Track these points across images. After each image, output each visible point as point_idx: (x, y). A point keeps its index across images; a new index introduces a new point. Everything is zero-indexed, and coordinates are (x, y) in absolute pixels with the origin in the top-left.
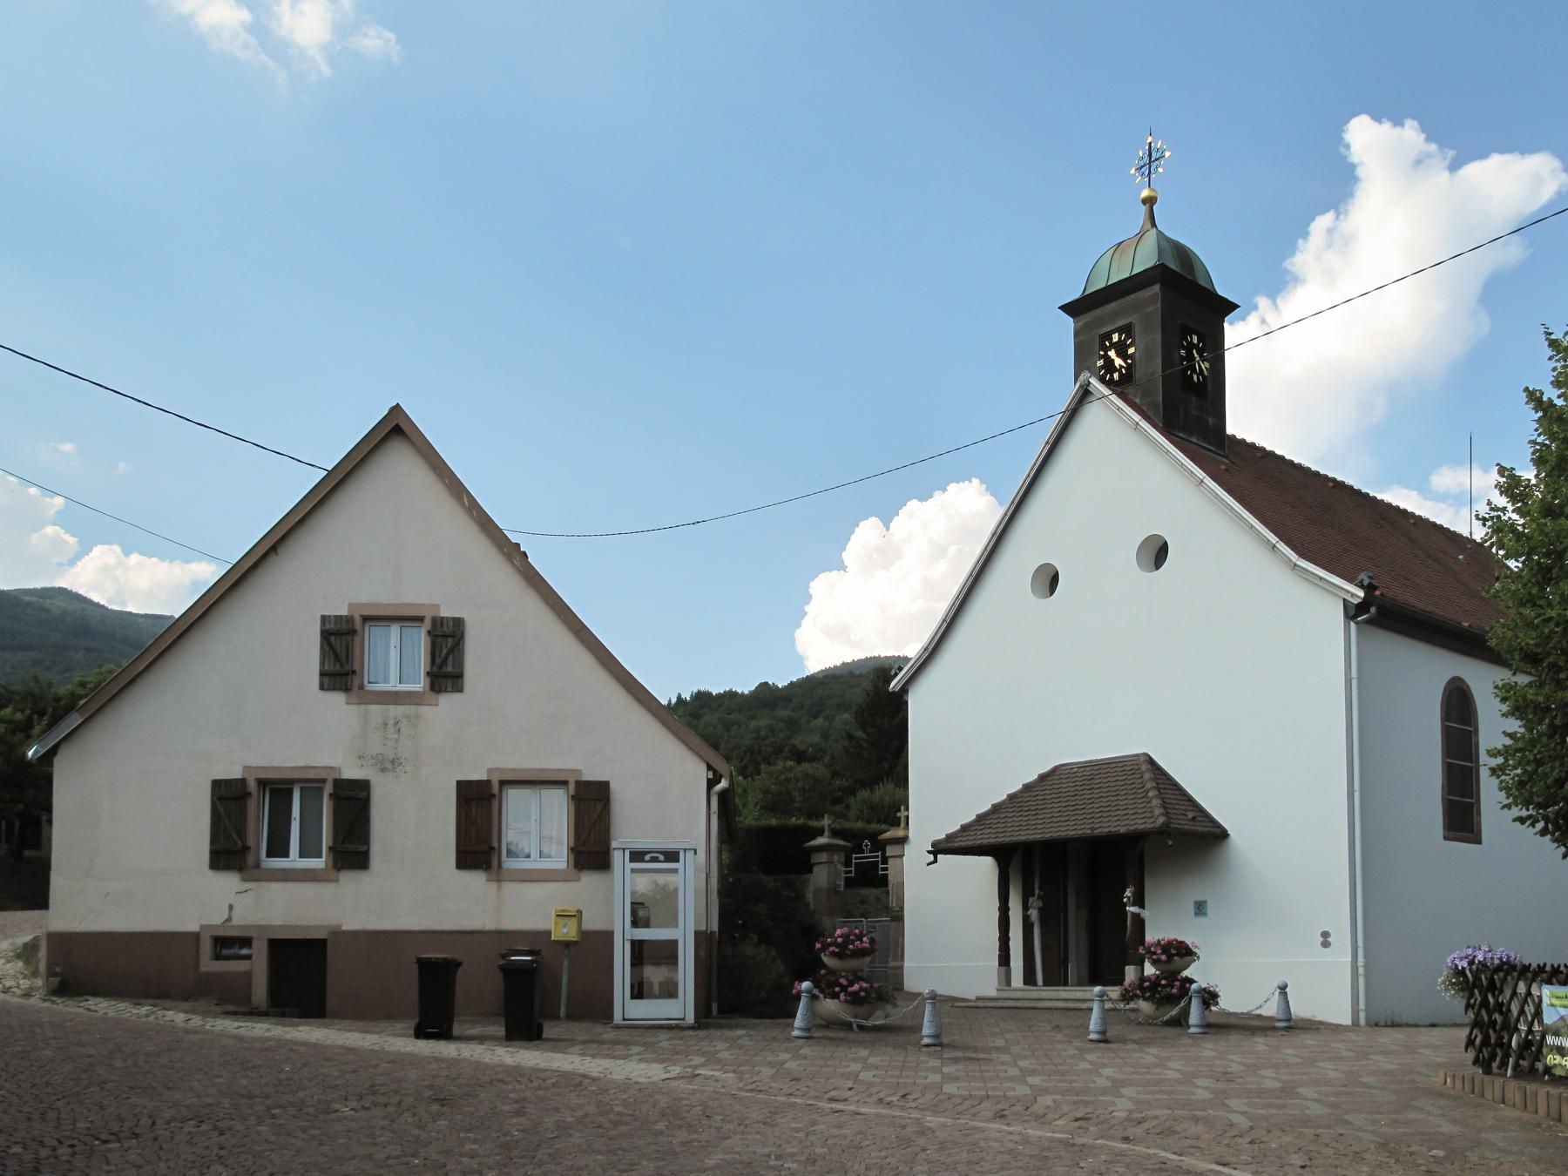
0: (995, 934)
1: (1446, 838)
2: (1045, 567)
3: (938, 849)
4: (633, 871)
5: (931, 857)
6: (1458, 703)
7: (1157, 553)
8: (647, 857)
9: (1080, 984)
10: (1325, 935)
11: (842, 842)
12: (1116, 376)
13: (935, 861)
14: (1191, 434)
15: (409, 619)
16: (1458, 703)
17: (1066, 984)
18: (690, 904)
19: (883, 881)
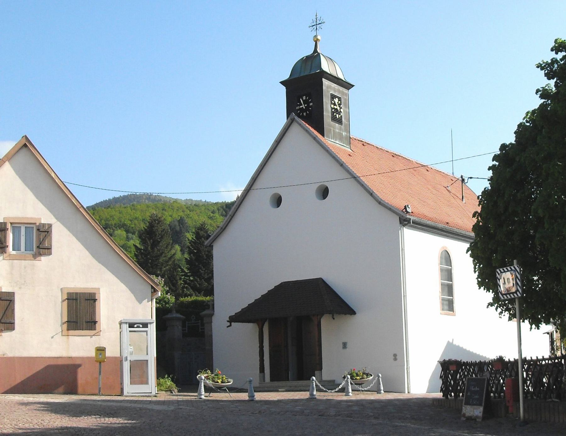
0: (258, 358)
1: (13, 293)
2: (275, 195)
3: (233, 319)
4: (130, 331)
5: (229, 324)
6: (446, 258)
7: (324, 193)
8: (135, 326)
9: (293, 380)
10: (395, 355)
11: (182, 316)
12: (305, 114)
13: (230, 325)
14: (336, 140)
15: (223, 229)
16: (446, 258)
17: (288, 380)
18: (147, 347)
19: (202, 335)
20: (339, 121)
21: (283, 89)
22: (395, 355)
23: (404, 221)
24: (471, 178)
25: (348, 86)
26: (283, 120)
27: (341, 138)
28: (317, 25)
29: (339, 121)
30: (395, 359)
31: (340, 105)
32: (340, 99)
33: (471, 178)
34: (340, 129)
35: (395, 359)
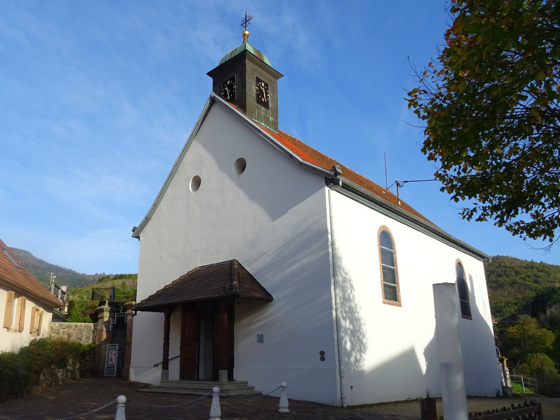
10: (322, 353)
20: (266, 105)
21: (211, 80)
22: (322, 353)
23: (331, 181)
24: (406, 182)
25: (278, 76)
27: (267, 122)
29: (266, 105)
30: (323, 359)
31: (266, 90)
32: (266, 85)
33: (406, 182)
35: (323, 359)
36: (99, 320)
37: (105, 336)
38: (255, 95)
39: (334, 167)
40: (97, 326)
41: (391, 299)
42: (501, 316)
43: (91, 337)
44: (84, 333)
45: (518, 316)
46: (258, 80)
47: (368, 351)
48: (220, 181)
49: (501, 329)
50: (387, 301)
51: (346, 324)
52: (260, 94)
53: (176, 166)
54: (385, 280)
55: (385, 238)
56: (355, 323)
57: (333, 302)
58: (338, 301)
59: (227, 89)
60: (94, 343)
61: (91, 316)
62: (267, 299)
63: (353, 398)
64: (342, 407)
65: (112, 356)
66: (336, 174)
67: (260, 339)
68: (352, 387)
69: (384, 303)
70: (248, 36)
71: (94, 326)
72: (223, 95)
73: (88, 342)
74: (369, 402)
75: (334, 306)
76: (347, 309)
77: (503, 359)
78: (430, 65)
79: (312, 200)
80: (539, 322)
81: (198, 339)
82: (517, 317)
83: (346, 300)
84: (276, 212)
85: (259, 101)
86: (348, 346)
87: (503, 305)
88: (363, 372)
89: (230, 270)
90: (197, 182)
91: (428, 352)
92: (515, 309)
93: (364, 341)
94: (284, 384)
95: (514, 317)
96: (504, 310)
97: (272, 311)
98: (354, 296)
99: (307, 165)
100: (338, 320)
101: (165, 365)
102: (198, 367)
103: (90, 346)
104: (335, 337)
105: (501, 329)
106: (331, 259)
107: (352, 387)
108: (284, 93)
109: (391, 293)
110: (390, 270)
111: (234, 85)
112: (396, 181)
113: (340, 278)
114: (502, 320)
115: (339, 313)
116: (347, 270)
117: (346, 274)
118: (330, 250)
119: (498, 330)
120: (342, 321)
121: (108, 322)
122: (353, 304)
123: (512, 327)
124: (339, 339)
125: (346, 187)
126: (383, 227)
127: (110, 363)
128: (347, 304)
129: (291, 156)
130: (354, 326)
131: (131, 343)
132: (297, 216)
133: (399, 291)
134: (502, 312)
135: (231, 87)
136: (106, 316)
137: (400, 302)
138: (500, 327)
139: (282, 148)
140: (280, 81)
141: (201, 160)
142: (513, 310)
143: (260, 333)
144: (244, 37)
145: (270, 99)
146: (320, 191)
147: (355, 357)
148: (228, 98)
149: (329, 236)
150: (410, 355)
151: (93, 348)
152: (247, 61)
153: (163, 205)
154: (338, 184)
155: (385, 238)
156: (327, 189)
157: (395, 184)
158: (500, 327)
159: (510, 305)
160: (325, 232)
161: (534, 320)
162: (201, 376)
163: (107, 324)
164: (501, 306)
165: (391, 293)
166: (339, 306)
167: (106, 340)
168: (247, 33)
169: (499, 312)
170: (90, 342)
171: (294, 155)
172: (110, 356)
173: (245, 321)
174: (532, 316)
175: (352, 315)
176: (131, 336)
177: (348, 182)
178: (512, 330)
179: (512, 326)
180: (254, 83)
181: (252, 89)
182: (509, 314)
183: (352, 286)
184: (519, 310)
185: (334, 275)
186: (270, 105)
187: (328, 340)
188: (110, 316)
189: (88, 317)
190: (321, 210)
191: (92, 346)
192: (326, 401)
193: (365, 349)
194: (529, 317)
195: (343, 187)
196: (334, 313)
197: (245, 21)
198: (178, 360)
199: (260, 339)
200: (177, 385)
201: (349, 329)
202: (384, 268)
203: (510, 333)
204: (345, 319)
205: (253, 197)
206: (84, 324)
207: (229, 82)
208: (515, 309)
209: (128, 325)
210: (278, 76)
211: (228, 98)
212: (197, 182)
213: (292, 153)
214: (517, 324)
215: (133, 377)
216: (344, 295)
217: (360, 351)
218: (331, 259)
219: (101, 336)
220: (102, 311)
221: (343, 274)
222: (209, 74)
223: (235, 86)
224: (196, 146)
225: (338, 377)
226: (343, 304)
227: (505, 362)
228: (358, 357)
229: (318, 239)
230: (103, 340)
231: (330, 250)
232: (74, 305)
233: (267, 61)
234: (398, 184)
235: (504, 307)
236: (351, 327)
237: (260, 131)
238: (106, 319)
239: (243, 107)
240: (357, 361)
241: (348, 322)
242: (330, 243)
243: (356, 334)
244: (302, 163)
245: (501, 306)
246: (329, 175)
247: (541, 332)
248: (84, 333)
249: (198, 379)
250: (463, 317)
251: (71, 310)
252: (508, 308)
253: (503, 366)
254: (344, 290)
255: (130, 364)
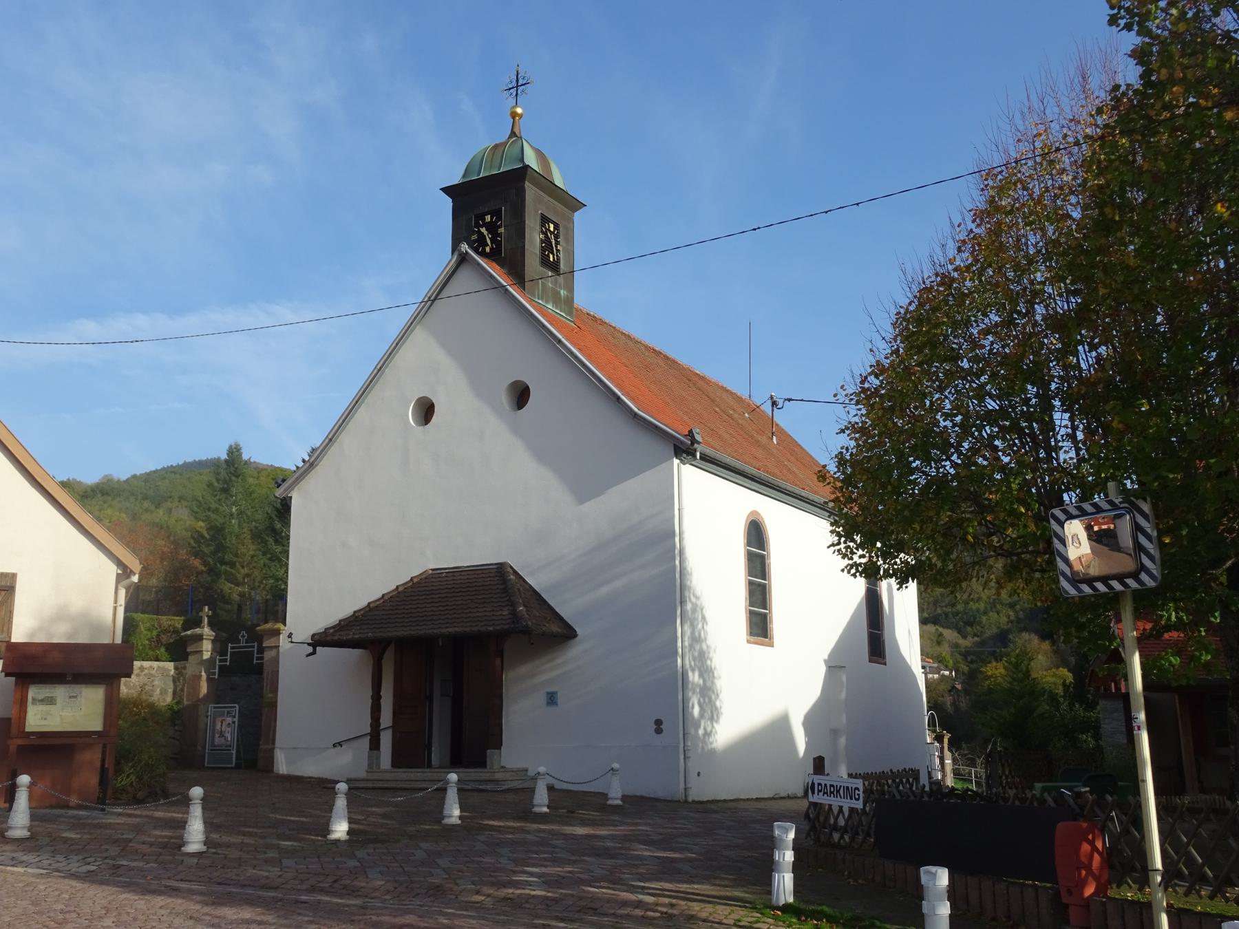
3: (318, 641)
5: (310, 649)
10: (658, 723)
13: (314, 653)
19: (259, 670)
20: (554, 267)
21: (448, 202)
22: (658, 723)
23: (684, 450)
24: (789, 400)
25: (575, 205)
26: (443, 256)
27: (557, 300)
28: (518, 86)
29: (554, 267)
30: (659, 731)
31: (557, 237)
32: (556, 226)
33: (789, 400)
34: (555, 283)
35: (659, 731)
36: (190, 658)
37: (204, 689)
38: (538, 251)
39: (691, 431)
40: (185, 668)
41: (758, 635)
42: (975, 635)
43: (171, 691)
44: (156, 683)
45: (1011, 636)
46: (545, 220)
47: (722, 720)
48: (469, 412)
49: (974, 666)
50: (752, 639)
51: (694, 677)
52: (547, 246)
53: (379, 370)
54: (751, 605)
55: (756, 533)
56: (706, 676)
57: (679, 644)
58: (686, 644)
59: (483, 230)
60: (178, 703)
61: (168, 648)
62: (567, 634)
63: (701, 790)
64: (686, 801)
65: (225, 728)
66: (694, 441)
67: (552, 699)
68: (699, 774)
69: (748, 642)
70: (521, 116)
71: (176, 668)
72: (475, 241)
73: (164, 700)
74: (718, 798)
75: (680, 650)
76: (696, 654)
77: (943, 737)
78: (842, 387)
79: (650, 477)
80: (1055, 652)
81: (430, 698)
82: (1010, 640)
83: (697, 640)
84: (584, 490)
85: (545, 262)
86: (696, 711)
87: (982, 606)
88: (713, 752)
89: (497, 583)
90: (426, 411)
91: (810, 722)
92: (1008, 617)
93: (718, 704)
94: (616, 766)
95: (1003, 638)
96: (984, 618)
97: (574, 653)
98: (706, 633)
99: (645, 419)
100: (684, 675)
101: (375, 745)
102: (429, 746)
103: (170, 708)
104: (680, 697)
105: (974, 666)
106: (678, 576)
107: (699, 774)
108: (588, 240)
109: (760, 627)
110: (760, 585)
111: (500, 227)
112: (772, 397)
113: (689, 606)
114: (976, 644)
115: (687, 662)
116: (698, 593)
117: (698, 598)
118: (677, 562)
119: (966, 669)
120: (690, 674)
121: (211, 661)
122: (704, 647)
123: (994, 664)
124: (685, 701)
125: (704, 458)
126: (754, 513)
127: (218, 741)
128: (697, 647)
129: (618, 398)
130: (704, 681)
131: (276, 702)
132: (620, 501)
133: (771, 621)
134: (980, 623)
135: (492, 228)
136: (207, 649)
137: (771, 638)
138: (972, 662)
139: (601, 381)
140: (577, 216)
141: (429, 365)
142: (1004, 620)
143: (550, 690)
144: (514, 118)
145: (561, 256)
146: (664, 465)
147: (705, 729)
148: (488, 249)
149: (677, 539)
150: (781, 725)
151: (179, 711)
152: (527, 184)
153: (345, 439)
154: (694, 456)
155: (756, 533)
156: (676, 461)
157: (769, 403)
158: (972, 662)
159: (999, 607)
160: (672, 534)
161: (1046, 646)
162: (435, 759)
163: (210, 663)
164: (978, 610)
165: (760, 627)
166: (687, 650)
167: (206, 696)
168: (519, 110)
169: (971, 625)
170: (169, 699)
171: (623, 397)
172: (218, 727)
173: (523, 670)
174: (1044, 636)
175: (702, 660)
176: (275, 689)
177: (709, 452)
178: (996, 670)
179: (996, 660)
180: (538, 228)
181: (534, 239)
182: (995, 631)
183: (704, 618)
184: (1019, 620)
185: (683, 602)
186: (562, 266)
187: (668, 699)
188: (214, 650)
189: (163, 650)
190: (666, 498)
191: (175, 708)
192: (661, 794)
193: (718, 718)
194: (1035, 640)
195: (701, 458)
196: (679, 661)
197: (514, 84)
198: (390, 732)
199: (552, 699)
200: (387, 776)
201: (698, 685)
202: (751, 583)
203: (989, 677)
204: (693, 671)
205: (541, 455)
206: (155, 664)
207: (488, 218)
208: (1008, 617)
209: (267, 669)
210: (575, 205)
211: (488, 249)
212: (426, 411)
213: (619, 394)
214: (1007, 655)
215: (282, 765)
216: (693, 633)
217: (712, 719)
218: (678, 576)
219: (196, 688)
220: (200, 638)
221: (693, 600)
222: (447, 190)
223: (502, 230)
224: (419, 334)
225: (682, 757)
226: (691, 646)
227: (946, 740)
228: (709, 729)
229: (660, 545)
230: (201, 696)
231: (677, 562)
232: (137, 626)
233: (558, 181)
234: (774, 404)
235: (985, 613)
236: (701, 682)
237: (560, 341)
238: (207, 655)
239: (518, 274)
240: (707, 734)
241: (697, 674)
242: (677, 552)
243: (708, 692)
244: (636, 414)
245: (978, 610)
246: (682, 442)
247: (1055, 675)
248: (156, 683)
249: (430, 766)
250: (870, 661)
251: (130, 635)
252: (993, 615)
253: (942, 749)
254: (693, 627)
255: (274, 743)
